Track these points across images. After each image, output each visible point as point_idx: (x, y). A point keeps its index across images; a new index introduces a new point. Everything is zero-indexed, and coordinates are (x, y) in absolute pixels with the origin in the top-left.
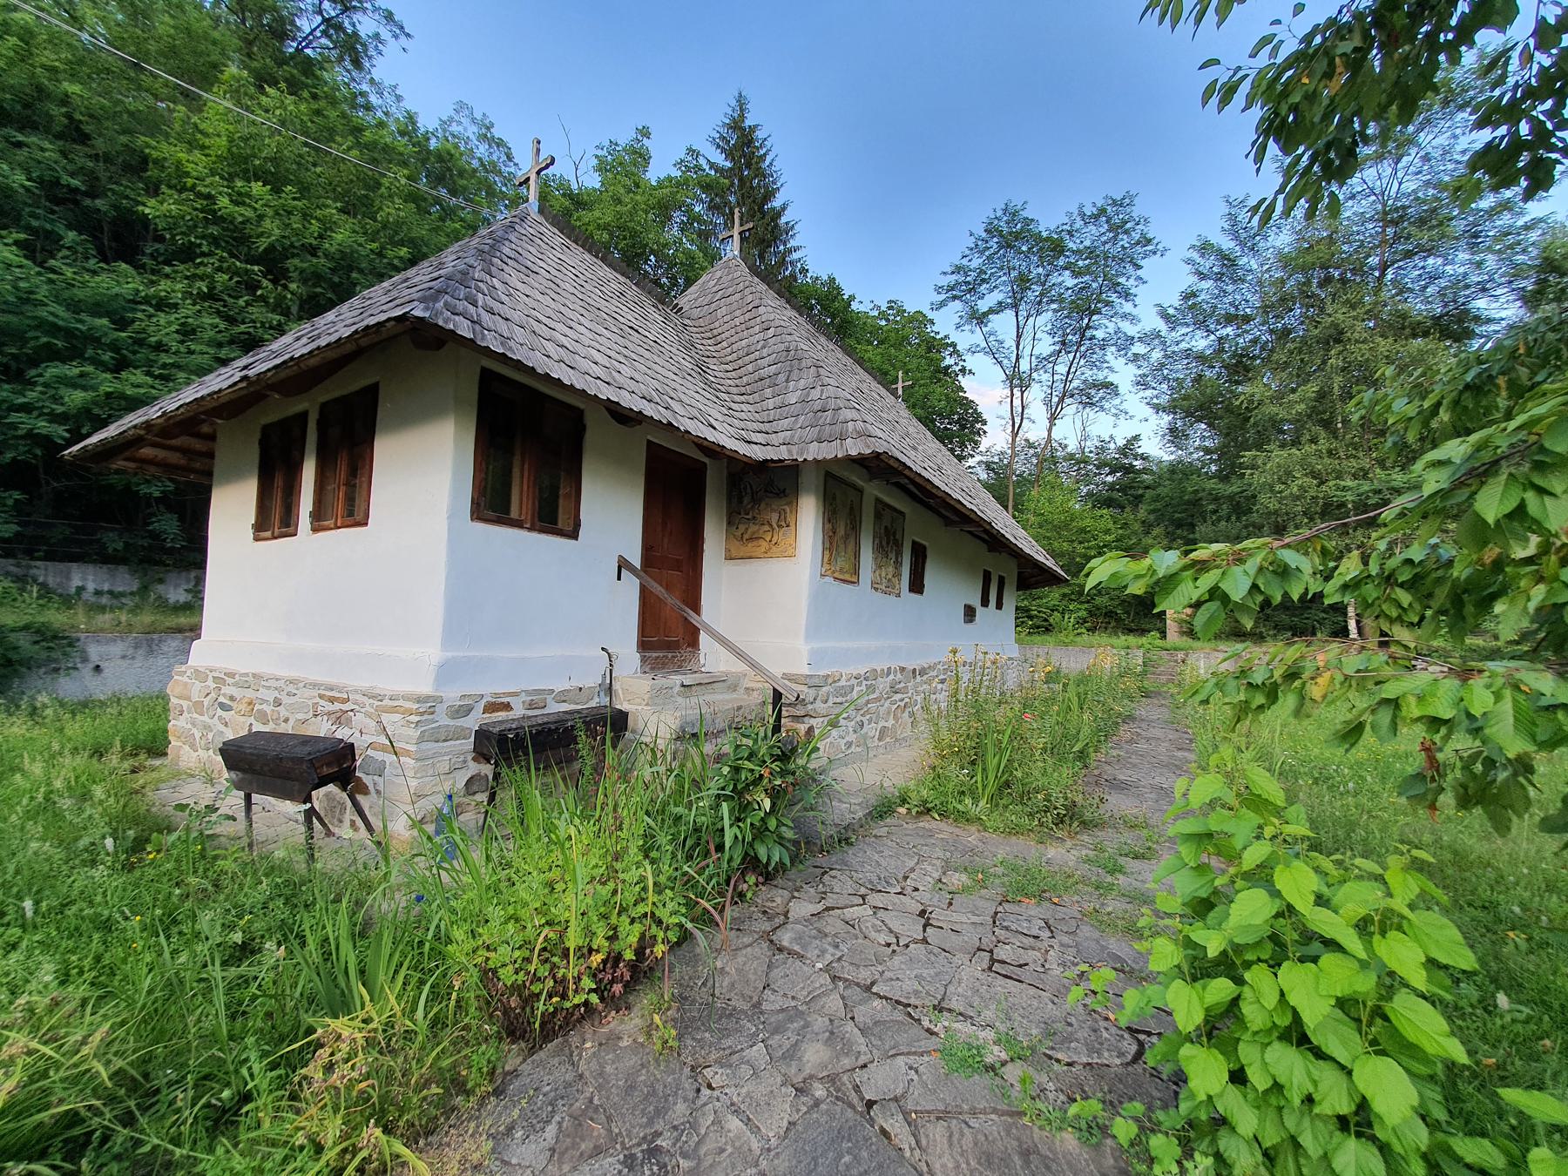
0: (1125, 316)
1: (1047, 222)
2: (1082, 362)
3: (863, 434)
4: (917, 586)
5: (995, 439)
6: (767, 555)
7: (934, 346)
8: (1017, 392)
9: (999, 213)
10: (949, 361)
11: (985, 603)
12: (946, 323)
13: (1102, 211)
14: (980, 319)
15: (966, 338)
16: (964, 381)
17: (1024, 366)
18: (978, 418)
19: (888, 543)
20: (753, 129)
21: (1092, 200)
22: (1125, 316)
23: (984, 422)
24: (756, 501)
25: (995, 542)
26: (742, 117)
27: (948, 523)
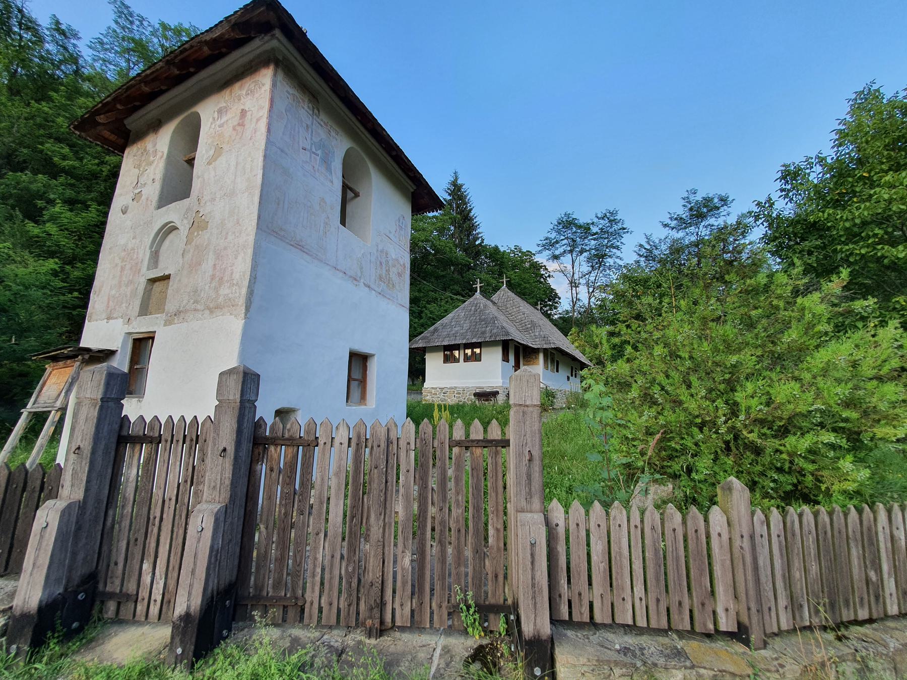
0: (617, 257)
1: (583, 220)
2: (601, 275)
3: (554, 343)
4: (557, 371)
5: (564, 305)
6: (533, 364)
7: (536, 267)
8: (574, 289)
9: (563, 216)
10: (543, 272)
11: (572, 376)
12: (541, 259)
13: (605, 215)
14: (556, 257)
15: (552, 266)
16: (550, 280)
17: (576, 277)
18: (556, 295)
19: (552, 361)
20: (461, 186)
21: (601, 210)
22: (617, 257)
23: (560, 298)
24: (530, 354)
25: (574, 359)
26: (456, 179)
27: (563, 355)
